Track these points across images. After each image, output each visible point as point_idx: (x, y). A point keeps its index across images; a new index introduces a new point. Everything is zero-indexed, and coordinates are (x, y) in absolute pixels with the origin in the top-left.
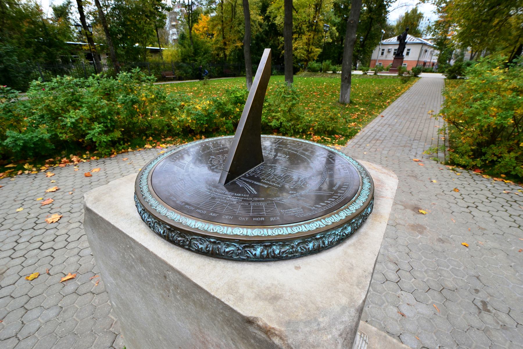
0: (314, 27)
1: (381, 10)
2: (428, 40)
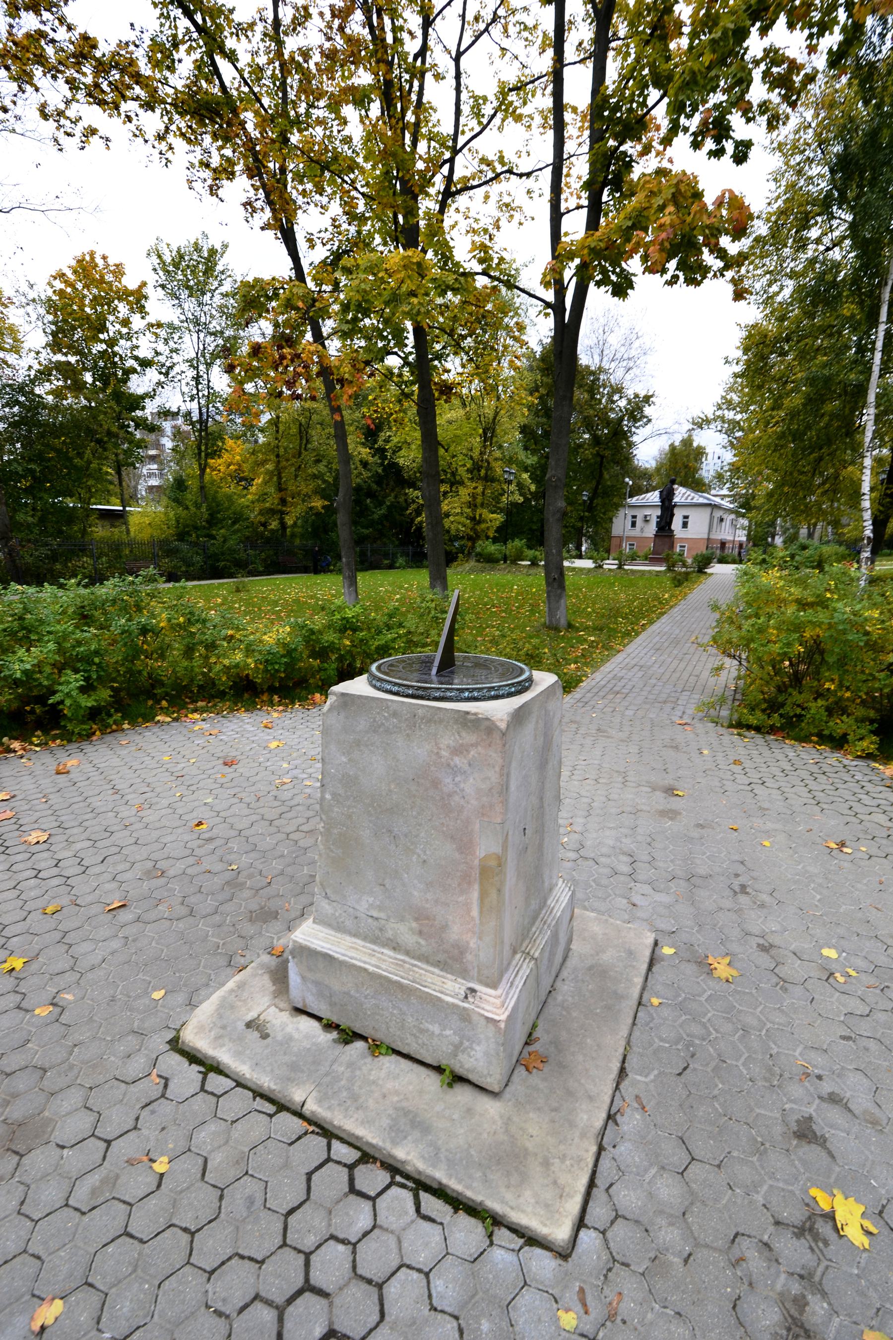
0: (483, 472)
1: (619, 441)
2: (723, 497)
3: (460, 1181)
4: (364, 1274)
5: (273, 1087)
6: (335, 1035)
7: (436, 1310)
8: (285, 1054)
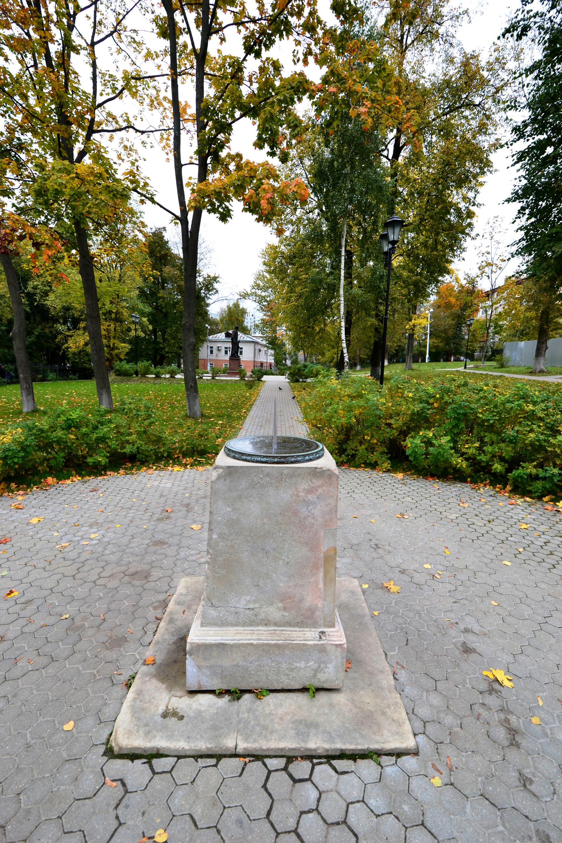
0: (113, 316)
1: (200, 302)
3: (351, 743)
4: (332, 822)
5: (210, 746)
6: (227, 698)
7: (379, 816)
8: (203, 723)
